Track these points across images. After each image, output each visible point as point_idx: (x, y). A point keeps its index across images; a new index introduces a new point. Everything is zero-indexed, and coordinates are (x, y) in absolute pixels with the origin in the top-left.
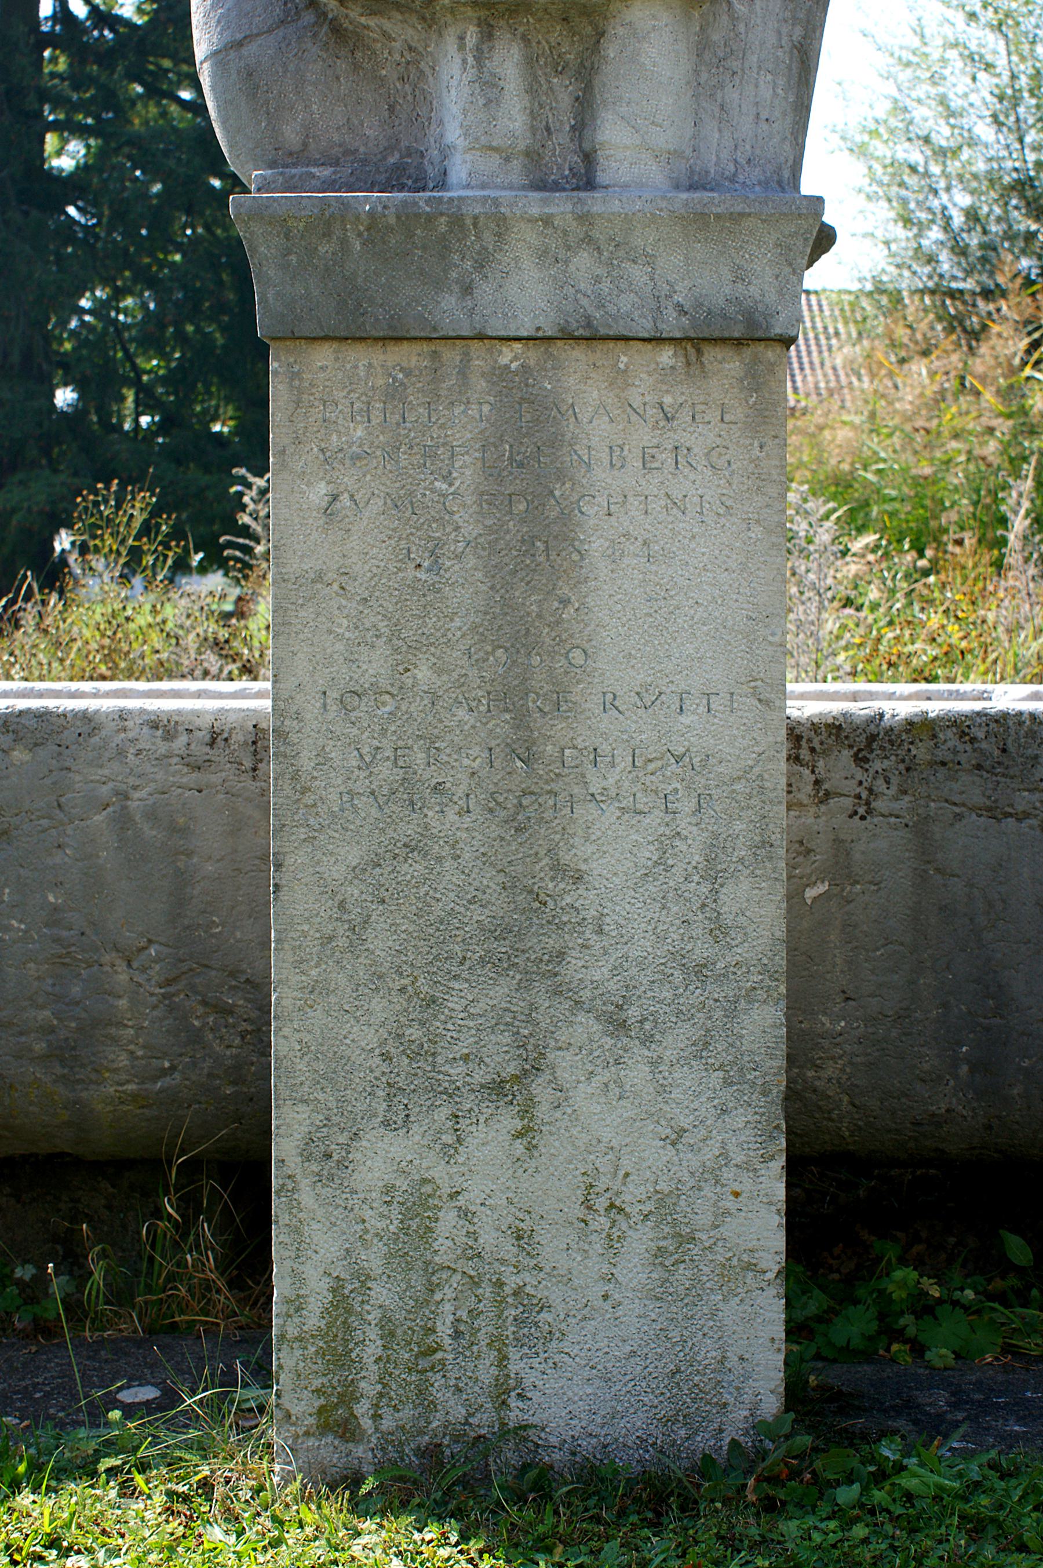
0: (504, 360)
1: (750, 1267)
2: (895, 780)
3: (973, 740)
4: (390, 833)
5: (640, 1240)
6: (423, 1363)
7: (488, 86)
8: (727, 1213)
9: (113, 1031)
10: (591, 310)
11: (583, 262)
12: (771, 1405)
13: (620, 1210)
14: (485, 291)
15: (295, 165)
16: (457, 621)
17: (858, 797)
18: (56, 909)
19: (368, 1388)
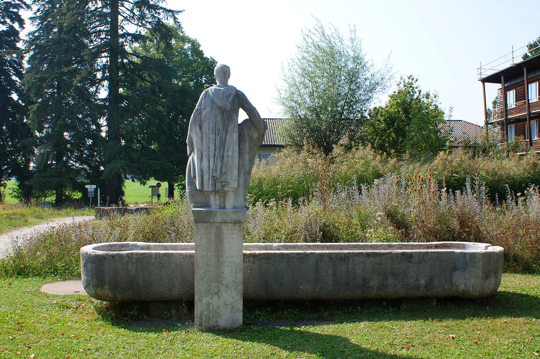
5: (229, 307)
7: (215, 199)
11: (224, 216)
12: (241, 323)
14: (215, 218)
19: (204, 322)
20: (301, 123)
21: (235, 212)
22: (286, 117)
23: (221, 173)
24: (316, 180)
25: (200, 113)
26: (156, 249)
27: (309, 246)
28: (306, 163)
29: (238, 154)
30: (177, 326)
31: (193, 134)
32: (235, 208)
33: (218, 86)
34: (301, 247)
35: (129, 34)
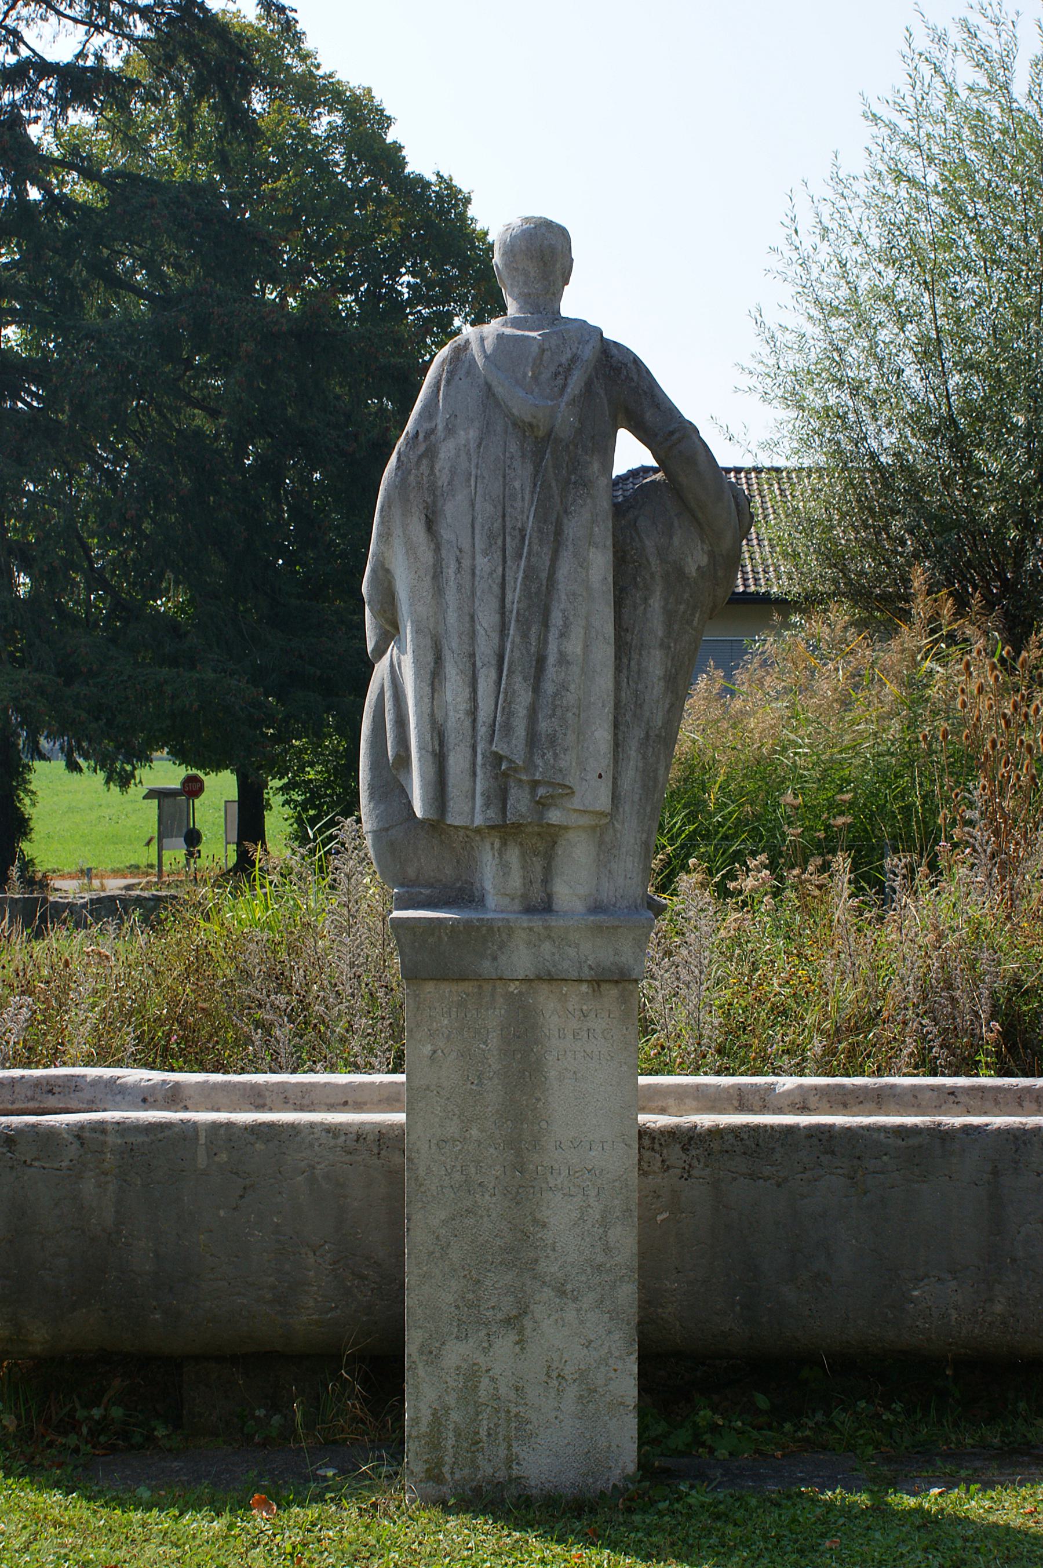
0: (511, 990)
1: (622, 1404)
2: (702, 1160)
3: (742, 1140)
4: (459, 1204)
5: (572, 1392)
6: (473, 1448)
7: (504, 867)
8: (611, 1379)
9: (306, 1288)
10: (550, 968)
11: (547, 947)
12: (631, 1468)
13: (563, 1378)
14: (503, 959)
15: (412, 886)
16: (490, 1109)
17: (684, 1168)
18: (278, 1225)
19: (448, 1459)
20: (879, 492)
21: (598, 929)
22: (807, 462)
23: (532, 739)
24: (966, 764)
25: (431, 453)
26: (211, 1101)
27: (952, 1092)
28: (915, 686)
29: (610, 651)
30: (317, 1478)
31: (393, 552)
32: (597, 908)
33: (516, 323)
34: (911, 1100)
35: (45, 69)
